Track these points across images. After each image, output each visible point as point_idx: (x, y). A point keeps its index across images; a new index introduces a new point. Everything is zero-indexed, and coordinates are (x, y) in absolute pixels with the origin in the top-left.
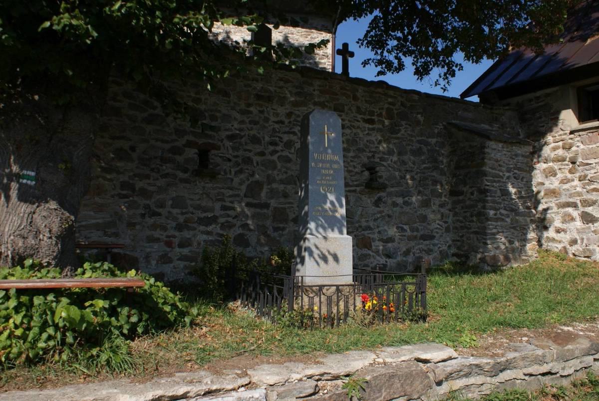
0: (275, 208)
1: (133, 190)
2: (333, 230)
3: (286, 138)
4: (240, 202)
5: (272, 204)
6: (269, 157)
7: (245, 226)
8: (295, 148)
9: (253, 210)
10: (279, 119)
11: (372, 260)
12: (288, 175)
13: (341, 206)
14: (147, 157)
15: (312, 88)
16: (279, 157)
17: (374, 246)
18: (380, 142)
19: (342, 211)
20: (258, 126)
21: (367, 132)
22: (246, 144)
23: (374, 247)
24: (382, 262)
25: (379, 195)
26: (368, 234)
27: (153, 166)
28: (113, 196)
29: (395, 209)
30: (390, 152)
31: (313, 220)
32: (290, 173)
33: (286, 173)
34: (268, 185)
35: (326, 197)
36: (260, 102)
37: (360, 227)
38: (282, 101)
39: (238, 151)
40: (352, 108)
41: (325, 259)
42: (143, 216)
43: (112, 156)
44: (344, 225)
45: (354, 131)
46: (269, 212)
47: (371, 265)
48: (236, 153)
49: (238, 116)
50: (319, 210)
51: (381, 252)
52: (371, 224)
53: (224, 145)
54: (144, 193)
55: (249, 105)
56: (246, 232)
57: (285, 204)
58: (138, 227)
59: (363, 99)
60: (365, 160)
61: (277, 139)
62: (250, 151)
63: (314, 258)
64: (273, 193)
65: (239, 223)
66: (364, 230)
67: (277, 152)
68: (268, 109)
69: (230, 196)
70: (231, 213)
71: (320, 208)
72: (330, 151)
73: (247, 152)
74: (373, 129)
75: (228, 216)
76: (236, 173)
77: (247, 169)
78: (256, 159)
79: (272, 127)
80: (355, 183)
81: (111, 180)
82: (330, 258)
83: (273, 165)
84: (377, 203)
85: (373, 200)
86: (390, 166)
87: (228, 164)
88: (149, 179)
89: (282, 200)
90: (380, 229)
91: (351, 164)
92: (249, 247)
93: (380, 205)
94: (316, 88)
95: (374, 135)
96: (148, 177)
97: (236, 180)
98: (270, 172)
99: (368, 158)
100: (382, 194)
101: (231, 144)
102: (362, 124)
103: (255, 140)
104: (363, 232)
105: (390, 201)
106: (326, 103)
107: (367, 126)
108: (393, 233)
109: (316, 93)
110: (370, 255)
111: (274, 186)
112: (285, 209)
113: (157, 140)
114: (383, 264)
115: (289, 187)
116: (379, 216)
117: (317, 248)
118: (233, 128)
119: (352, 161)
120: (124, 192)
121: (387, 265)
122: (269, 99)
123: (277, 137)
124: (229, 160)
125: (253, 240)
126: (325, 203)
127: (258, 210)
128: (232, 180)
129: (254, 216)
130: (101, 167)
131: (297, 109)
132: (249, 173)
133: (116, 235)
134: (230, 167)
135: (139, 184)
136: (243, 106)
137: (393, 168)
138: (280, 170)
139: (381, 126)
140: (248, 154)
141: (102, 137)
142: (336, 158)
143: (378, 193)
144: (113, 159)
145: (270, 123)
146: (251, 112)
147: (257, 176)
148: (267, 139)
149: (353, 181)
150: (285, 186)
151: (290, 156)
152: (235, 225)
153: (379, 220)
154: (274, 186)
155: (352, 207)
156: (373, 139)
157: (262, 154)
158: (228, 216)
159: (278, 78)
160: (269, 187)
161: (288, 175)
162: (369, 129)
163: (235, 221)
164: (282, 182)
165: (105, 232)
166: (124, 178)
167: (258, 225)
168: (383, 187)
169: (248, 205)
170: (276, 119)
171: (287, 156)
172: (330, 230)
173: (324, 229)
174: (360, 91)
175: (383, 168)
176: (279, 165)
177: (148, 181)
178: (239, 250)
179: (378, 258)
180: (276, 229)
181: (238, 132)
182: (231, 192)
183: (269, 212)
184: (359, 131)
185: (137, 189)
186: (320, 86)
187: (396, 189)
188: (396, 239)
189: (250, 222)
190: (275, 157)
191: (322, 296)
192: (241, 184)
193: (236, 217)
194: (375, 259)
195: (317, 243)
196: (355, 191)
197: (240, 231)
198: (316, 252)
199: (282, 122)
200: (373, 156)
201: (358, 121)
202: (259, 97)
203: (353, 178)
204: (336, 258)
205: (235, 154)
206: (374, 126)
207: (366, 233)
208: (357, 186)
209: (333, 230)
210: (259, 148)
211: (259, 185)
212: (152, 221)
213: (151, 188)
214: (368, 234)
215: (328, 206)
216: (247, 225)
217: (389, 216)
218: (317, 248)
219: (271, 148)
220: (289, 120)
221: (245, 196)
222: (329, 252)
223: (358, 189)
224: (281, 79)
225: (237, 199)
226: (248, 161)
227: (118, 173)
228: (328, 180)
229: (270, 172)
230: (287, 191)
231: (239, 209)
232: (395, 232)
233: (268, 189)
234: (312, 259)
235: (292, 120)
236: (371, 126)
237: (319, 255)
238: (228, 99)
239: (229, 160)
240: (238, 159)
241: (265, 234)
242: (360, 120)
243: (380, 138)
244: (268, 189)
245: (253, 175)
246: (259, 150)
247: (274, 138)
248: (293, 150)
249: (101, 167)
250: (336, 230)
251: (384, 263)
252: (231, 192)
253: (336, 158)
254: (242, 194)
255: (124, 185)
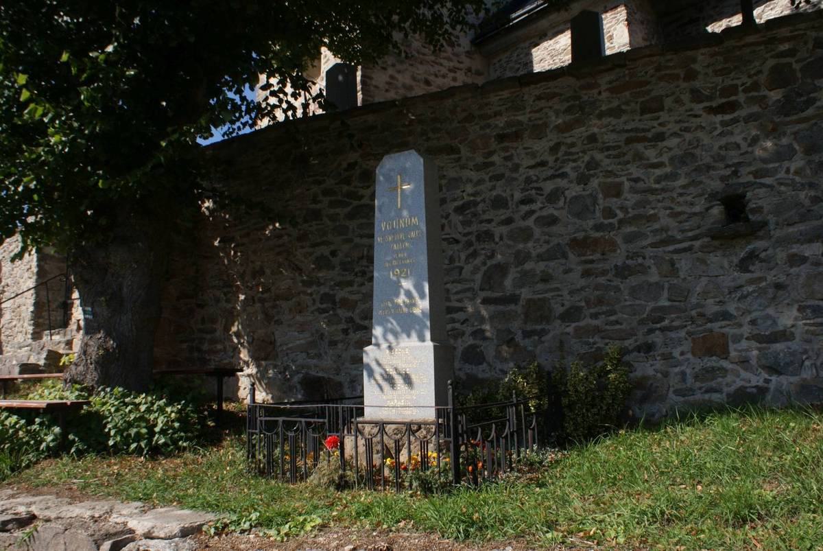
0: (529, 301)
1: (334, 303)
2: (409, 336)
3: (549, 187)
4: (473, 299)
5: (523, 296)
6: (523, 224)
7: (478, 334)
8: (566, 198)
9: (492, 308)
10: (538, 160)
11: (729, 378)
12: (552, 244)
13: (422, 296)
14: (349, 259)
15: (595, 91)
16: (537, 220)
17: (736, 350)
18: (755, 141)
19: (424, 305)
20: (504, 180)
21: (718, 132)
22: (484, 212)
23: (733, 354)
24: (754, 383)
25: (751, 247)
26: (721, 327)
27: (356, 270)
28: (312, 312)
29: (794, 270)
30: (783, 155)
31: (380, 324)
32: (555, 241)
33: (547, 242)
34: (516, 267)
35: (398, 286)
36: (506, 144)
37: (701, 315)
38: (538, 131)
39: (470, 226)
40: (682, 97)
41: (390, 380)
42: (345, 332)
43: (313, 266)
44: (425, 326)
45: (688, 136)
46: (519, 309)
47: (726, 389)
48: (468, 230)
49: (474, 175)
50: (388, 307)
51: (754, 362)
52: (732, 308)
53: (450, 222)
54: (345, 303)
55: (491, 154)
56: (478, 342)
57: (546, 291)
58: (340, 346)
59: (710, 71)
60: (717, 185)
61: (534, 192)
62: (489, 221)
63: (375, 380)
64: (526, 278)
65: (469, 330)
66: (711, 321)
67: (533, 212)
68: (518, 151)
69: (457, 293)
70: (459, 316)
71: (390, 305)
72: (405, 213)
73: (483, 224)
74: (735, 121)
75: (453, 321)
76: (467, 258)
77: (483, 249)
78: (499, 231)
79: (524, 176)
80: (690, 234)
81: (311, 294)
82: (399, 381)
83: (526, 234)
84: (744, 266)
85: (736, 260)
86: (781, 184)
87: (456, 247)
88: (352, 286)
89: (540, 286)
90: (754, 315)
91: (681, 199)
92: (481, 364)
93: (751, 268)
94: (604, 87)
95: (737, 131)
96: (350, 284)
97: (468, 268)
98: (521, 246)
99: (723, 179)
100: (759, 244)
101: (461, 217)
102: (706, 119)
103: (499, 203)
104: (709, 325)
105: (781, 255)
106: (623, 107)
107: (719, 118)
108: (790, 322)
109: (605, 95)
110: (722, 369)
111: (528, 266)
112: (544, 300)
113: (361, 236)
114: (756, 387)
115: (552, 264)
116: (750, 289)
117: (379, 364)
118: (464, 194)
119: (681, 195)
120: (324, 306)
121: (767, 389)
122: (517, 136)
123: (532, 189)
124: (457, 242)
125: (490, 353)
126: (397, 295)
127: (501, 308)
128: (461, 268)
129: (492, 318)
130: (303, 282)
131: (566, 135)
132: (485, 254)
133: (319, 356)
134: (458, 250)
135: (341, 294)
136: (480, 159)
137: (793, 185)
138: (538, 240)
139: (755, 109)
140: (485, 227)
141: (302, 247)
142: (415, 221)
143: (749, 243)
144: (313, 269)
145: (521, 170)
146: (493, 164)
147: (499, 256)
148: (518, 195)
149: (683, 231)
150: (546, 263)
151: (556, 213)
152: (463, 334)
153: (749, 299)
154: (528, 266)
155: (685, 279)
156: (738, 139)
157: (509, 221)
158: (453, 321)
159: (533, 99)
160: (519, 269)
161: (552, 244)
162: (723, 124)
163: (464, 327)
164: (541, 258)
165: (308, 354)
166: (324, 290)
167: (498, 330)
168: (757, 230)
169: (486, 301)
170: (532, 162)
171: (552, 215)
172: (404, 336)
173: (396, 335)
174: (700, 58)
175: (762, 191)
176: (537, 232)
177: (350, 289)
178: (468, 368)
179: (743, 374)
180: (527, 334)
181: (472, 198)
182: (459, 287)
183: (519, 309)
184: (700, 134)
185: (337, 300)
186: (610, 82)
187: (801, 227)
188: (798, 333)
189: (487, 327)
190: (530, 222)
191: (360, 437)
192: (474, 272)
193: (466, 320)
194: (738, 376)
195: (378, 358)
196: (690, 249)
197: (471, 341)
198: (377, 371)
199: (543, 164)
200: (735, 173)
201: (696, 116)
202: (501, 138)
203: (686, 225)
204: (407, 380)
205: (465, 231)
206: (735, 115)
207: (716, 326)
208: (695, 238)
209: (409, 336)
210: (503, 214)
211: (502, 269)
212: (358, 336)
213: (355, 297)
214: (721, 327)
215: (402, 299)
216: (483, 331)
217: (779, 286)
218: (379, 364)
219: (525, 208)
220: (554, 158)
221: (482, 289)
222: (396, 369)
223: (697, 244)
224: (539, 98)
225: (469, 294)
226: (488, 236)
227: (319, 284)
228: (401, 258)
229: (521, 246)
230: (550, 271)
231: (470, 309)
232: (796, 319)
233: (517, 272)
234: (373, 382)
235: (560, 154)
236: (727, 117)
237: (382, 375)
238: (457, 156)
239: (457, 242)
240: (469, 237)
241: (510, 342)
242: (701, 112)
243: (754, 132)
244: (517, 272)
245: (492, 256)
246: (503, 217)
247: (527, 193)
248: (561, 203)
249: (303, 282)
250: (414, 335)
251: (761, 383)
252: (459, 287)
253: (415, 221)
254: (476, 287)
255: (326, 298)
